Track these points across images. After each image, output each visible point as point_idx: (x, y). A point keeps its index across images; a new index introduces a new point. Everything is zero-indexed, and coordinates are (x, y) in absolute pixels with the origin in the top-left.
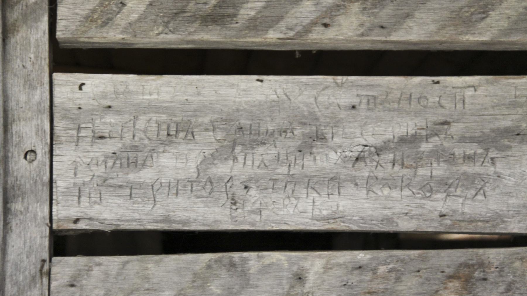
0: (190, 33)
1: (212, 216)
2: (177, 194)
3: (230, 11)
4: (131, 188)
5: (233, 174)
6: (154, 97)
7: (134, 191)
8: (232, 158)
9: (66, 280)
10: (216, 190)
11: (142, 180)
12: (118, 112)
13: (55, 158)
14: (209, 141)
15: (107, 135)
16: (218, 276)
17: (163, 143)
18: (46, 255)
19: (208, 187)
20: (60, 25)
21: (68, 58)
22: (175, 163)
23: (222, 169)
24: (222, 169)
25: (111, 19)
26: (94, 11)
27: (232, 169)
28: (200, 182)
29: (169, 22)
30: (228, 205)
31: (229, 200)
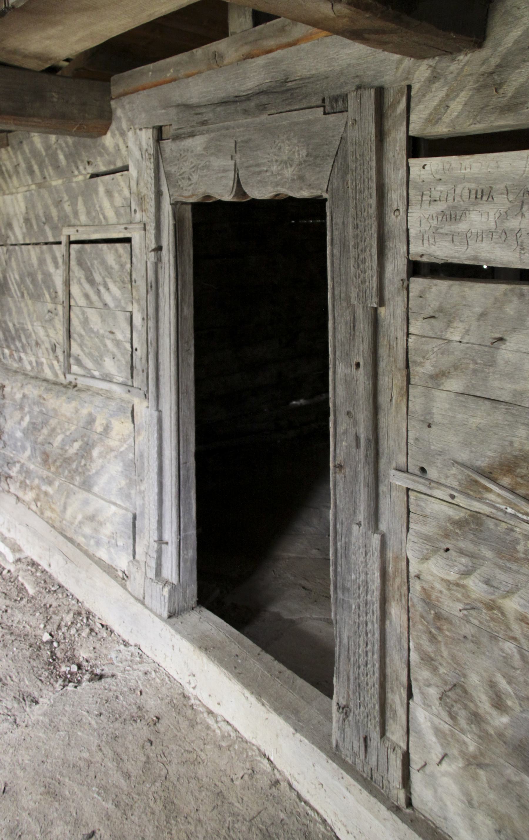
0: (492, 122)
1: (506, 258)
2: (482, 240)
3: (523, 99)
4: (453, 235)
5: (521, 227)
6: (468, 170)
7: (454, 237)
8: (520, 214)
9: (417, 293)
10: (509, 238)
11: (460, 230)
12: (445, 183)
13: (409, 215)
14: (501, 203)
15: (438, 199)
16: (511, 302)
17: (473, 204)
18: (405, 276)
19: (503, 236)
20: (411, 126)
21: (417, 147)
22: (479, 219)
23: (513, 223)
24: (513, 223)
25: (440, 119)
26: (431, 114)
27: (520, 223)
28: (497, 232)
29: (477, 115)
30: (518, 250)
31: (519, 247)
